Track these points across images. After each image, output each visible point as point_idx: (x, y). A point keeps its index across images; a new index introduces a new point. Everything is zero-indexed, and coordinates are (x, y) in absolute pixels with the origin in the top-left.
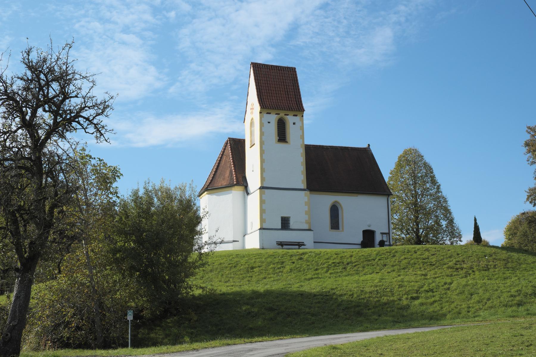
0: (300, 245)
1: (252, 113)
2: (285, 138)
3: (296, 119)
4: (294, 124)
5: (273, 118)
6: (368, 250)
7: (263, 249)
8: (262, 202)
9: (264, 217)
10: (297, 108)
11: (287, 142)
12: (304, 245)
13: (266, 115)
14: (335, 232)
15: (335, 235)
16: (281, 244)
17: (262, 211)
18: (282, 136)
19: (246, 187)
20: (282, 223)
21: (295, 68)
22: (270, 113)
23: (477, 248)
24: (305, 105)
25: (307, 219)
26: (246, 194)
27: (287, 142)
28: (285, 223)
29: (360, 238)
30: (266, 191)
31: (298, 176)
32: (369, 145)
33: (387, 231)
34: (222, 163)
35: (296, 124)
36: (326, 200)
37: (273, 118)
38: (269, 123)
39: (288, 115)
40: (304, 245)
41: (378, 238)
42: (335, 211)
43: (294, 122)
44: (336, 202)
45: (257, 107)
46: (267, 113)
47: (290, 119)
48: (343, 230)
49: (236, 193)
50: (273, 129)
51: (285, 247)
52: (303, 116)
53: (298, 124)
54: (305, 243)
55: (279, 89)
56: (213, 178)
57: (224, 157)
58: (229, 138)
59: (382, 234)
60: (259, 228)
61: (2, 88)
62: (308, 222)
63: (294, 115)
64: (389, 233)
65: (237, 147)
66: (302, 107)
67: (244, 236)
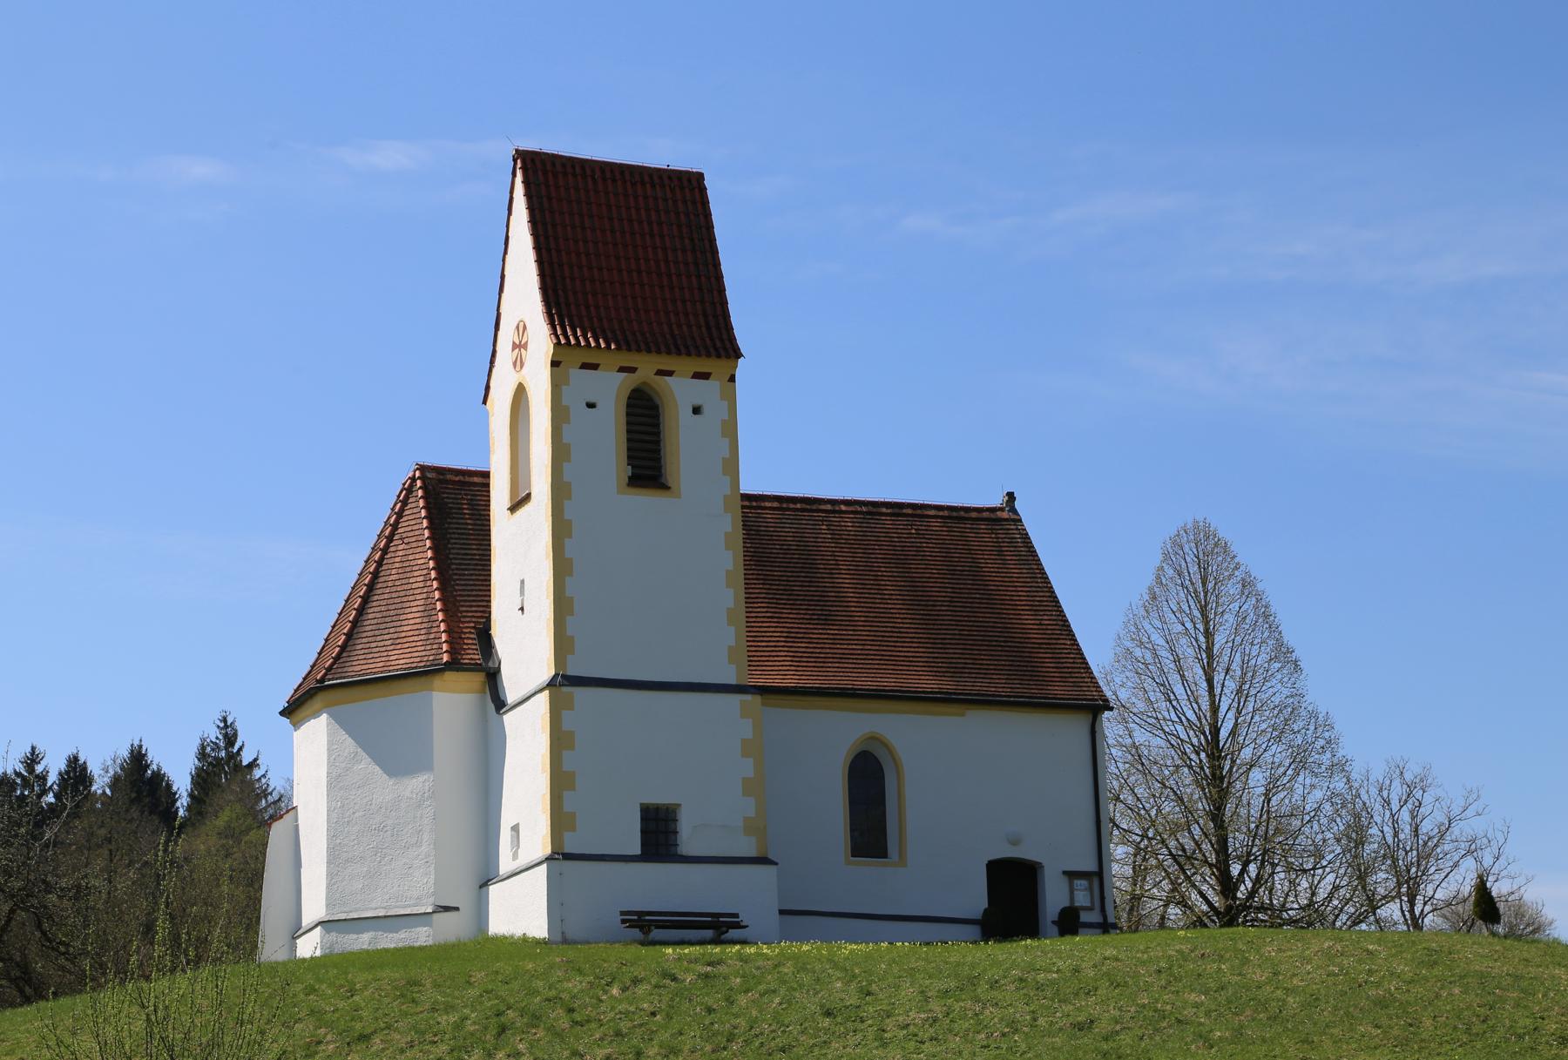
1: (519, 363)
3: (705, 392)
5: (608, 387)
7: (565, 941)
8: (560, 740)
10: (715, 342)
11: (668, 488)
13: (576, 375)
14: (868, 869)
15: (870, 883)
16: (647, 925)
17: (561, 781)
18: (647, 465)
19: (492, 677)
22: (595, 367)
26: (491, 707)
27: (668, 488)
28: (659, 834)
29: (975, 899)
30: (579, 693)
32: (1011, 496)
33: (1090, 866)
34: (391, 573)
35: (705, 410)
36: (837, 732)
37: (608, 387)
38: (591, 405)
39: (670, 373)
40: (738, 926)
42: (868, 779)
43: (698, 402)
44: (874, 739)
46: (585, 366)
47: (681, 390)
48: (902, 860)
49: (450, 703)
50: (606, 433)
51: (656, 934)
52: (732, 379)
54: (744, 918)
55: (632, 262)
57: (398, 548)
59: (1072, 875)
60: (548, 851)
62: (750, 827)
63: (697, 376)
65: (451, 508)
66: (732, 339)
67: (485, 885)
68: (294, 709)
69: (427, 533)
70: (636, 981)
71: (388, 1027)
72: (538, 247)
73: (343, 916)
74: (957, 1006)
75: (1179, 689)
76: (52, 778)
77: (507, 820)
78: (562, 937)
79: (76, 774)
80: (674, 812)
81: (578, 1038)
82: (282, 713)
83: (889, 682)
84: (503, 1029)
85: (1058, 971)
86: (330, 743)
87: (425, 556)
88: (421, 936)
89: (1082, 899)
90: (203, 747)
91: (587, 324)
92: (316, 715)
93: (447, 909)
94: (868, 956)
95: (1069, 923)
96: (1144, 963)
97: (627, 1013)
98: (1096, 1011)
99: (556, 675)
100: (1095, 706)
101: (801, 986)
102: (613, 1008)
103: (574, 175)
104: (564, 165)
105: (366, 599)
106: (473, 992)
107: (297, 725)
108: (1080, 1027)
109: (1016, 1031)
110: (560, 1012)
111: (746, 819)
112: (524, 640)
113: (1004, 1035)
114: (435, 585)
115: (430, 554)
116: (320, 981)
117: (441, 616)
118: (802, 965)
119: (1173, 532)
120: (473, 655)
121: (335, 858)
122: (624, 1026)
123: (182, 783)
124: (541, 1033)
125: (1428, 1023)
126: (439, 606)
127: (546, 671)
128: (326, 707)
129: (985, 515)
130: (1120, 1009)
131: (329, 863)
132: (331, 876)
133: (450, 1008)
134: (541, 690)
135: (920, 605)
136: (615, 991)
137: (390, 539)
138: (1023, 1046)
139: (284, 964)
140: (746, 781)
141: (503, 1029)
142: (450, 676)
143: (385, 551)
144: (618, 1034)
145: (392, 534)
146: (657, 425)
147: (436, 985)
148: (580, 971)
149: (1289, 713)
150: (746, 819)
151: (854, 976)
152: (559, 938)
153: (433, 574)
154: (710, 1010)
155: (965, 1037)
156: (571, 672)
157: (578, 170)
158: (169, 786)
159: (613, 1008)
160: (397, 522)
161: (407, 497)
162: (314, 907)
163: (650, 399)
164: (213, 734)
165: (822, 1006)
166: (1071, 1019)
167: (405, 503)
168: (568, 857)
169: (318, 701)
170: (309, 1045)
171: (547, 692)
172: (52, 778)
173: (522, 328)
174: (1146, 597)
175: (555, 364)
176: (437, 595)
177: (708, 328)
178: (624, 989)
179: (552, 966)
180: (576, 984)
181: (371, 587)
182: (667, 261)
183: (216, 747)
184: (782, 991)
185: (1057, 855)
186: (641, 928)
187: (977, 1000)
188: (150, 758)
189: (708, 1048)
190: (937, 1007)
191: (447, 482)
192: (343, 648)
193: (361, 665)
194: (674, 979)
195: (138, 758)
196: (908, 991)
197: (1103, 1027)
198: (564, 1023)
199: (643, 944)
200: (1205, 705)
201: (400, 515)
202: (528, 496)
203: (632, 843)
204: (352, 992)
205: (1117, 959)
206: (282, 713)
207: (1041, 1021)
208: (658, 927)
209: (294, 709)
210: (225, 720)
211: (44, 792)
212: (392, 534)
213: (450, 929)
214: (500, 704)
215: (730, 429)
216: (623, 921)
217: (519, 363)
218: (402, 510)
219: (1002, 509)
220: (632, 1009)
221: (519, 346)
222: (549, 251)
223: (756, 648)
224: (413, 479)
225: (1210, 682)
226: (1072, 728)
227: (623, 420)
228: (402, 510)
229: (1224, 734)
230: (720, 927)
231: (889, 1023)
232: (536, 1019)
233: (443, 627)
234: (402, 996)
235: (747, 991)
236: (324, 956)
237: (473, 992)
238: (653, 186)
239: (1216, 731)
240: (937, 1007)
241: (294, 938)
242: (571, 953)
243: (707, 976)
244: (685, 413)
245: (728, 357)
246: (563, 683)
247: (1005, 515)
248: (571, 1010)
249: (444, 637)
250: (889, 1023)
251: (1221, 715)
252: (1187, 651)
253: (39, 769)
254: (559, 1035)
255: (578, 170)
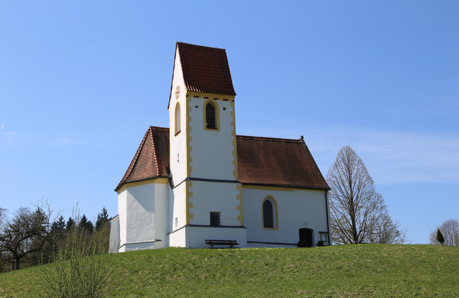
0: (232, 244)
1: (177, 97)
2: (214, 124)
3: (227, 104)
4: (224, 109)
5: (201, 102)
6: (305, 250)
7: (190, 248)
8: (189, 195)
9: (191, 212)
10: (228, 90)
11: (217, 129)
12: (237, 244)
13: (193, 99)
14: (268, 231)
15: (269, 235)
16: (212, 243)
17: (189, 205)
18: (211, 122)
19: (170, 179)
20: (211, 219)
21: (225, 50)
22: (198, 97)
23: (440, 248)
24: (236, 91)
25: (239, 214)
26: (170, 187)
27: (217, 129)
28: (215, 220)
29: (297, 239)
30: (194, 182)
31: (228, 166)
32: (302, 137)
33: (325, 230)
34: (144, 153)
35: (227, 108)
36: (261, 195)
37: (201, 102)
38: (197, 107)
39: (217, 99)
40: (237, 244)
41: (316, 238)
42: (268, 207)
43: (225, 107)
44: (270, 197)
45: (184, 90)
46: (195, 97)
47: (220, 104)
48: (277, 229)
49: (159, 186)
50: (200, 115)
51: (215, 246)
52: (234, 101)
53: (229, 109)
54: (238, 242)
55: (207, 71)
56: (133, 169)
57: (145, 147)
58: (152, 127)
59: (321, 233)
60: (186, 224)
61: (132, 296)
62: (239, 218)
63: (225, 100)
64: (328, 232)
65: (159, 138)
66: (233, 91)
67: (168, 234)
68: (118, 189)
69: (153, 143)
70: (211, 257)
71: (143, 269)
72: (183, 66)
73: (131, 243)
74: (303, 263)
75: (343, 188)
76: (66, 223)
77: (175, 217)
78: (189, 247)
79: (71, 222)
80: (219, 214)
81: (197, 271)
82: (115, 190)
83: (273, 182)
84: (175, 269)
85: (329, 254)
86: (127, 197)
87: (152, 149)
88: (152, 248)
89: (324, 239)
90: (99, 216)
91: (195, 86)
92: (124, 190)
93: (158, 240)
94: (274, 250)
95: (321, 244)
96: (352, 252)
97: (210, 265)
98: (342, 264)
99: (188, 177)
100: (326, 189)
101: (258, 258)
102: (206, 264)
103: (192, 49)
104: (189, 46)
105: (137, 160)
106: (167, 260)
107: (119, 193)
108: (339, 268)
109: (321, 269)
110: (191, 264)
111: (238, 216)
112: (179, 169)
113: (318, 270)
114: (155, 156)
115: (154, 148)
116: (125, 257)
117: (157, 164)
118: (257, 253)
119: (341, 149)
120: (165, 174)
121: (129, 227)
122: (210, 268)
123: (94, 224)
124: (186, 270)
125: (438, 267)
126: (156, 161)
127: (185, 177)
128: (127, 187)
129: (296, 141)
130: (349, 263)
131: (127, 229)
132: (128, 232)
133: (160, 264)
134: (184, 182)
135: (281, 164)
136: (206, 259)
137: (143, 145)
138: (324, 273)
139: (115, 254)
140: (238, 206)
141: (175, 269)
142: (159, 179)
143: (142, 148)
144: (208, 270)
145: (144, 144)
146: (214, 113)
147: (156, 258)
148: (196, 254)
149: (372, 193)
150: (238, 216)
151: (272, 255)
152: (189, 247)
153: (155, 153)
154: (233, 264)
155: (307, 271)
156: (191, 177)
157: (193, 48)
158: (92, 225)
159: (206, 264)
160: (145, 140)
161: (148, 134)
162: (123, 241)
163: (212, 106)
164: (102, 212)
165: (265, 263)
166: (336, 266)
167: (147, 136)
168: (191, 226)
169: (124, 187)
170: (121, 273)
171: (185, 182)
172: (66, 223)
173: (178, 88)
174: (334, 165)
175: (187, 96)
176: (156, 158)
177: (227, 88)
178: (209, 259)
179: (188, 253)
180: (195, 257)
181: (138, 157)
182: (216, 71)
183: (102, 215)
184: (253, 259)
185: (317, 227)
186: (211, 244)
187: (308, 261)
188: (87, 218)
189: (234, 274)
190: (298, 263)
191: (158, 130)
192: (131, 173)
193: (136, 177)
194: (222, 256)
195: (84, 219)
196: (288, 259)
197: (345, 268)
198: (193, 267)
199: (211, 248)
200: (349, 192)
201: (146, 139)
202: (180, 131)
203: (209, 223)
204: (133, 260)
205: (344, 251)
206: (115, 190)
207: (327, 267)
208: (215, 244)
209: (118, 189)
210: (104, 209)
211: (64, 226)
212: (144, 144)
213: (158, 246)
214: (172, 187)
215: (233, 114)
216: (206, 243)
217: (177, 97)
218: (146, 137)
219: (300, 140)
220: (211, 264)
221: (178, 93)
222: (185, 67)
223: (240, 173)
224: (149, 130)
225: (351, 187)
226: (321, 194)
227: (205, 111)
228: (146, 137)
229: (354, 199)
230: (232, 244)
231: (285, 267)
232: (184, 267)
233: (157, 167)
234: (147, 260)
235: (243, 259)
236: (126, 252)
237: (167, 260)
238: (212, 52)
239: (352, 199)
240: (298, 263)
241: (118, 249)
242: (193, 250)
243: (231, 255)
244: (221, 109)
245: (233, 95)
246: (189, 179)
247: (301, 142)
248: (194, 264)
249: (157, 169)
250: (285, 267)
251: (354, 193)
252: (344, 178)
253: (63, 221)
254: (191, 271)
255: (193, 48)
